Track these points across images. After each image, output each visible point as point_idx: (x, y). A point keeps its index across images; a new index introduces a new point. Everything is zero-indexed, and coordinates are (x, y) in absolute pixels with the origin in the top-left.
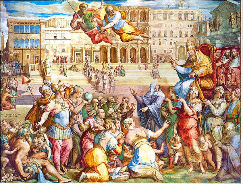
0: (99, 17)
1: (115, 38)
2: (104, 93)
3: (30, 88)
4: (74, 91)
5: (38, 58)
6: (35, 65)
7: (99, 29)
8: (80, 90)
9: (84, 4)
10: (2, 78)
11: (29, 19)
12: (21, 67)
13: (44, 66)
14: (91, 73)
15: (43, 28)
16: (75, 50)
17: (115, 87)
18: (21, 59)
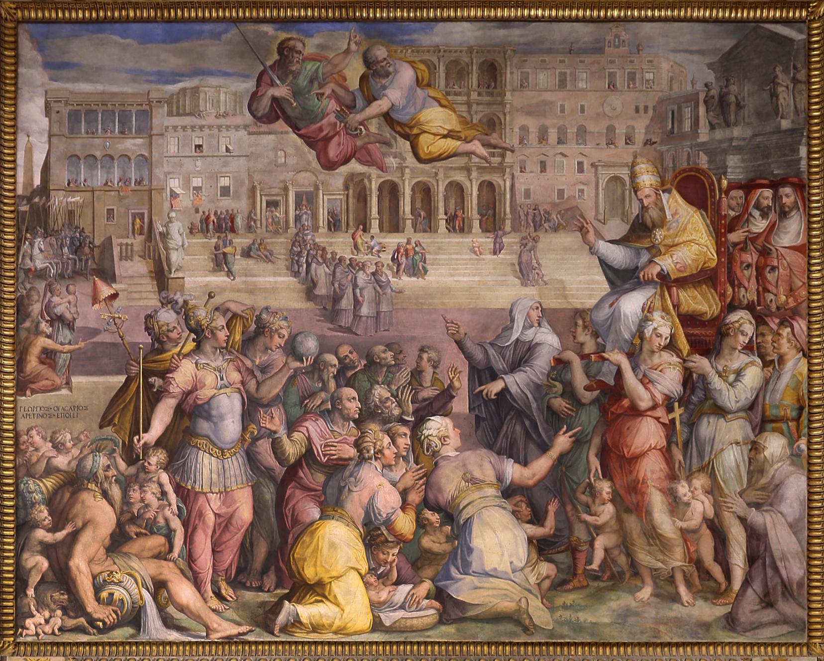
1: (393, 150)
2: (356, 334)
4: (258, 328)
5: (142, 219)
6: (133, 241)
7: (341, 122)
9: (294, 39)
10: (28, 286)
11: (115, 89)
12: (87, 250)
13: (161, 245)
14: (314, 265)
15: (161, 118)
18: (90, 221)
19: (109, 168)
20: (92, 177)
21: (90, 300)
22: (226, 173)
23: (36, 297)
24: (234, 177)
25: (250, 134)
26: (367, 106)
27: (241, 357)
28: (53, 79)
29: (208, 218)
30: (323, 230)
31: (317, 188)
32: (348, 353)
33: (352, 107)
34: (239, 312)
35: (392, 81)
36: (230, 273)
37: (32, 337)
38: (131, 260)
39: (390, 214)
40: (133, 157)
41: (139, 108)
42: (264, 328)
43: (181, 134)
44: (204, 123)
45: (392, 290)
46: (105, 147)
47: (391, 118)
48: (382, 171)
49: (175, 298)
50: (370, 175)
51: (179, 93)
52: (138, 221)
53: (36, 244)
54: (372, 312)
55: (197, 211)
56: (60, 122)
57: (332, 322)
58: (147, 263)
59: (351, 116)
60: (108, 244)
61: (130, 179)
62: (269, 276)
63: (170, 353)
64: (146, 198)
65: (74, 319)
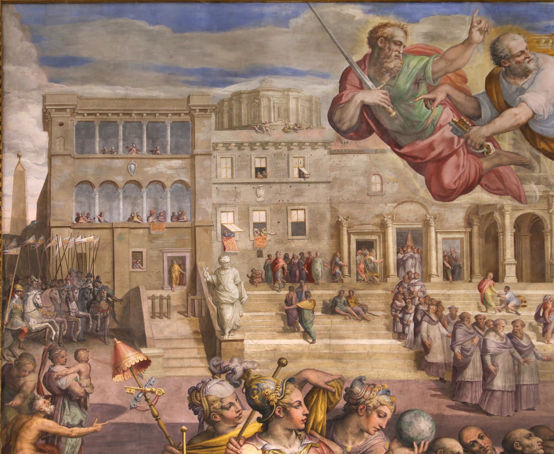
0: (460, 82)
1: (536, 174)
2: (488, 414)
3: (149, 395)
4: (349, 404)
5: (182, 265)
6: (170, 293)
7: (459, 137)
8: (377, 398)
9: (392, 25)
10: (18, 352)
11: (142, 93)
12: (104, 305)
13: (209, 299)
14: (425, 325)
15: (206, 132)
16: (349, 227)
17: (540, 386)
18: (107, 267)
19: (136, 198)
20: (111, 210)
21: (110, 370)
22: (300, 204)
23: (30, 366)
24: (311, 211)
25: (331, 153)
26: (497, 117)
27: (327, 441)
28: (52, 80)
29: (275, 263)
30: (437, 279)
31: (427, 224)
32: (475, 438)
33: (475, 117)
34: (322, 384)
35: (532, 83)
36: (307, 334)
37: (24, 418)
38: (169, 318)
39: (532, 259)
40: (168, 184)
41: (176, 118)
42: (358, 404)
43: (235, 153)
44: (267, 139)
45: (537, 357)
46: (128, 170)
47: (532, 132)
48: (520, 201)
49: (232, 366)
50: (502, 207)
51: (231, 99)
52: (176, 267)
53: (31, 297)
54: (510, 385)
55: (260, 254)
56: (65, 137)
57: (452, 398)
58: (190, 321)
59: (475, 129)
60: (133, 298)
61: (165, 213)
62: (362, 337)
63: (226, 437)
64: (188, 237)
65: (87, 394)
